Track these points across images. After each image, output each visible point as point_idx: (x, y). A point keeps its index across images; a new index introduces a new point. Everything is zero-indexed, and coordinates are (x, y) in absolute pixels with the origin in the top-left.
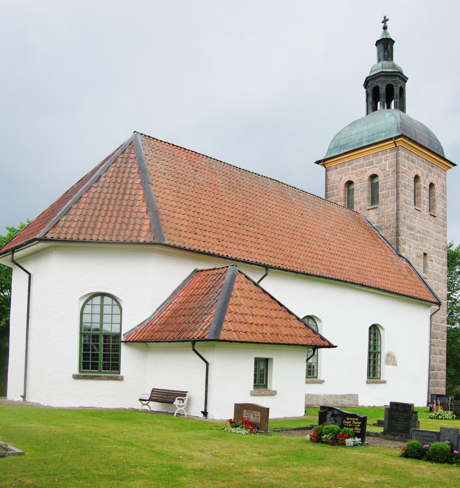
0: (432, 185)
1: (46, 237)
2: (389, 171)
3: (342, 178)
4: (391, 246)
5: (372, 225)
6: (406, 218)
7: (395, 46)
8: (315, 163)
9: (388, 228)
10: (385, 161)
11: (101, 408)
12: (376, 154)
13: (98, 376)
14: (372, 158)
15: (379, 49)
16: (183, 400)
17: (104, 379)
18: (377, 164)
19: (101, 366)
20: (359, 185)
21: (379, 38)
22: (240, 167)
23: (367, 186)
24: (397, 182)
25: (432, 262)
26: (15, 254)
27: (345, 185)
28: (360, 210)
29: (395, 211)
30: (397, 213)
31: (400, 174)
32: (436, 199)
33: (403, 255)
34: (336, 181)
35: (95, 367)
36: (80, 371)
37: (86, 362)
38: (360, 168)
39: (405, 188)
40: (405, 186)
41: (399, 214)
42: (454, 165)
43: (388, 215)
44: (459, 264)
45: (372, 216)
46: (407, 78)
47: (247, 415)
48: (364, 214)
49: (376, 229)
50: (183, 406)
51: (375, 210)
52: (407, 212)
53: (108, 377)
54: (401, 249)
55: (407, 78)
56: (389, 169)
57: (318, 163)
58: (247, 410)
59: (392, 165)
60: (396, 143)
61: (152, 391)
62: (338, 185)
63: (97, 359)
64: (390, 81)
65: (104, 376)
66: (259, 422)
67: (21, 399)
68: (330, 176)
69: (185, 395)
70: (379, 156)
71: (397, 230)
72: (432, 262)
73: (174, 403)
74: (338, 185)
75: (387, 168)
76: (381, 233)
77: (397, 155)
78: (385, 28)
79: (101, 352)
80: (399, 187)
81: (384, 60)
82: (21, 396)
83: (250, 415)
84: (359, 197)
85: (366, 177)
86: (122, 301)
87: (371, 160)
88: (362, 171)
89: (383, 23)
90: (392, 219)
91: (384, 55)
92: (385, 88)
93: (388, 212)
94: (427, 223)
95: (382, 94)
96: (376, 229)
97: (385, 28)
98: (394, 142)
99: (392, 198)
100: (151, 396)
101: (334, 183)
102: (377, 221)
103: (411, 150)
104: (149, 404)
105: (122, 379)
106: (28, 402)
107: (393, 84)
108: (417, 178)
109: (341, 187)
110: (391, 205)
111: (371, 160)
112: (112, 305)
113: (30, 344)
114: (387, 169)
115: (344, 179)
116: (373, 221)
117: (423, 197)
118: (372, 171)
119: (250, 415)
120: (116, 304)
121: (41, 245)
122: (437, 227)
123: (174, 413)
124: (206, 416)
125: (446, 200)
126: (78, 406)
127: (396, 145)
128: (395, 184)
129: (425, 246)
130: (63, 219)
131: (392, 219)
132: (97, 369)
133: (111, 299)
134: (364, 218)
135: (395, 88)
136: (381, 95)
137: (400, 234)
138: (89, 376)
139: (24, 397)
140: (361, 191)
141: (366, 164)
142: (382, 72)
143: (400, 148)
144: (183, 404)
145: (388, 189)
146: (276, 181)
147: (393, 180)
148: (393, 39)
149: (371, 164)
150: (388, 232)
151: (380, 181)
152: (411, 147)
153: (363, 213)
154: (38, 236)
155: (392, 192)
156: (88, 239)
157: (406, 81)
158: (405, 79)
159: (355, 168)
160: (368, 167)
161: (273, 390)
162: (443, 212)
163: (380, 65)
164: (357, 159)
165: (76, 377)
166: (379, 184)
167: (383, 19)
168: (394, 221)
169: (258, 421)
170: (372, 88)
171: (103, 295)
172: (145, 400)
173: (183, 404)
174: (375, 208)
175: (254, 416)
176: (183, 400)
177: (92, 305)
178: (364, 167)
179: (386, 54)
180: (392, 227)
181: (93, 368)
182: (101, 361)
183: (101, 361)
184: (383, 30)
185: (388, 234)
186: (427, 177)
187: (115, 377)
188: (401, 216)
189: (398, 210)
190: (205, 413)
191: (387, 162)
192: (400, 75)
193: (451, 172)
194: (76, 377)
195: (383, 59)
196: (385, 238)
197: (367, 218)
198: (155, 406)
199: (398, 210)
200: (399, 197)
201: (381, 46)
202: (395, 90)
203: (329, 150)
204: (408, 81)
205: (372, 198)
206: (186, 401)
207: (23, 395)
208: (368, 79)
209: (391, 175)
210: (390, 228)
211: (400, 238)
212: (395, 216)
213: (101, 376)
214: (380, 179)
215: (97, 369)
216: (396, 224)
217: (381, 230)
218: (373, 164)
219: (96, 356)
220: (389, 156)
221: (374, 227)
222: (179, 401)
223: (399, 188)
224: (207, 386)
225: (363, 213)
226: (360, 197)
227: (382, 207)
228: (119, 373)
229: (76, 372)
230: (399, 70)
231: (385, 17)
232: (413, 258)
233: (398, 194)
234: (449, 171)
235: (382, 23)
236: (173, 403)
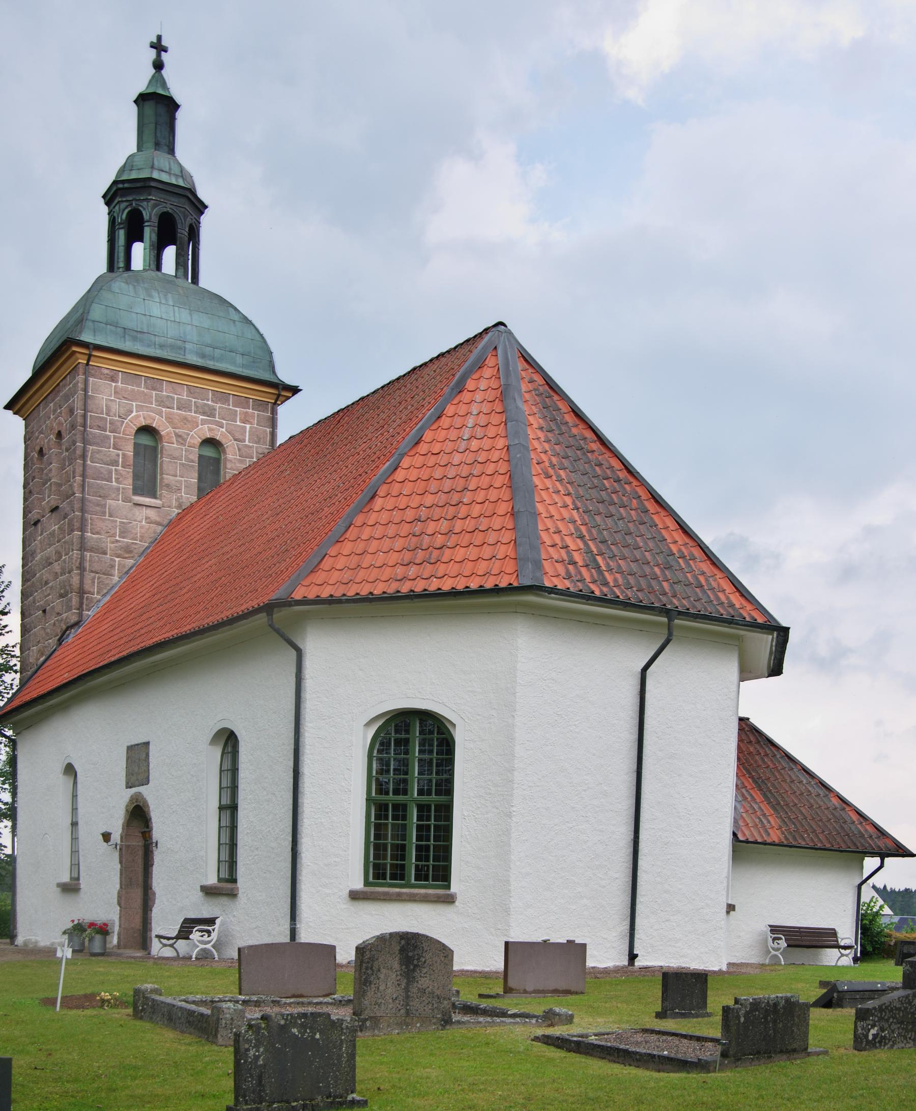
1: (292, 598)
2: (251, 447)
12: (222, 398)
16: (209, 932)
35: (399, 874)
36: (367, 883)
46: (206, 207)
50: (209, 942)
55: (206, 207)
60: (92, 358)
78: (158, 66)
85: (196, 436)
97: (158, 66)
105: (450, 900)
115: (137, 417)
118: (210, 430)
127: (88, 361)
139: (293, 933)
144: (209, 939)
148: (178, 99)
157: (202, 213)
158: (200, 207)
173: (209, 939)
176: (209, 932)
181: (393, 877)
184: (154, 71)
192: (190, 196)
219: (400, 851)
222: (200, 934)
228: (448, 887)
229: (358, 884)
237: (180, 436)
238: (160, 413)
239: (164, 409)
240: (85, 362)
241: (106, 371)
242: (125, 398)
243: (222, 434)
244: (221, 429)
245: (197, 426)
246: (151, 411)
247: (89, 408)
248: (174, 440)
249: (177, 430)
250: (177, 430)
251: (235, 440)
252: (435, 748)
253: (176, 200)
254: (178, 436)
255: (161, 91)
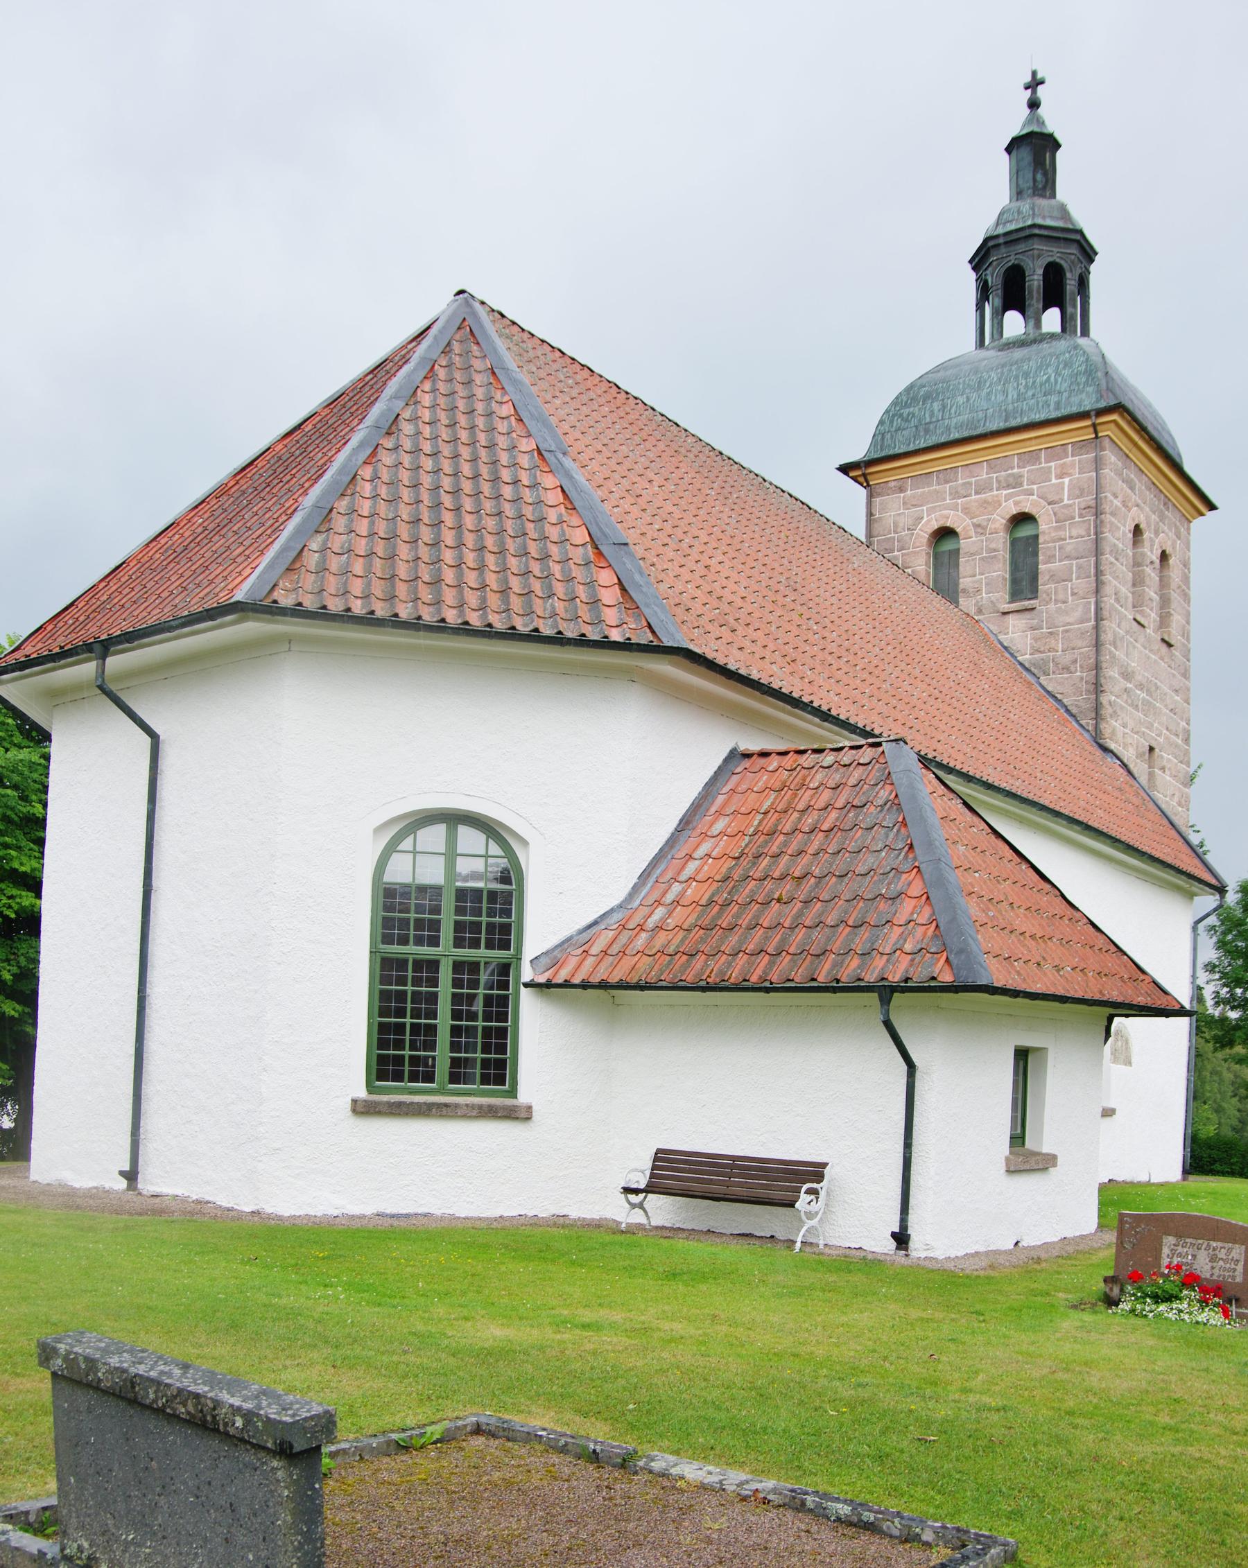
0: (1164, 556)
1: (275, 602)
2: (1071, 505)
3: (922, 518)
4: (1077, 721)
5: (1015, 658)
6: (1118, 643)
7: (1060, 155)
8: (838, 469)
9: (1066, 669)
10: (1060, 476)
11: (454, 1218)
12: (1033, 457)
13: (446, 1105)
14: (1019, 467)
15: (1018, 162)
17: (465, 1117)
18: (1033, 483)
19: (442, 1069)
20: (974, 542)
21: (1016, 130)
22: (720, 449)
23: (1001, 546)
24: (1097, 541)
25: (1164, 772)
26: (109, 660)
27: (929, 540)
28: (980, 611)
29: (1088, 620)
30: (1097, 628)
31: (1107, 518)
32: (1172, 598)
33: (1112, 746)
34: (901, 525)
37: (388, 1056)
38: (977, 493)
39: (1117, 559)
40: (1116, 553)
41: (1104, 632)
42: (1212, 507)
43: (1067, 631)
44: (7, 819)
45: (1016, 632)
47: (1180, 1255)
48: (992, 627)
49: (1027, 670)
51: (1027, 615)
52: (1119, 626)
53: (480, 1107)
54: (1106, 728)
55: (1096, 254)
56: (1071, 502)
57: (845, 469)
58: (1179, 1235)
59: (1082, 491)
60: (1099, 428)
61: (656, 1159)
62: (907, 538)
63: (431, 1046)
64: (1054, 253)
65: (467, 1105)
66: (1239, 1279)
67: (122, 1184)
68: (883, 510)
69: (819, 1177)
70: (1040, 463)
71: (1097, 676)
72: (1164, 772)
73: (797, 1205)
74: (908, 538)
75: (1066, 497)
76: (1044, 683)
77: (1098, 464)
78: (1034, 104)
79: (444, 1021)
80: (1102, 554)
81: (1034, 194)
82: (122, 1173)
83: (1194, 1256)
84: (975, 576)
85: (999, 520)
86: (525, 843)
87: (1016, 470)
88: (985, 502)
89: (1029, 91)
90: (1079, 643)
91: (1035, 180)
92: (1041, 271)
93: (1069, 624)
94: (1155, 661)
95: (1035, 288)
96: (1027, 670)
97: (1034, 104)
98: (1094, 426)
99: (1084, 584)
100: (652, 1176)
101: (896, 532)
102: (1032, 647)
103: (1130, 455)
104: (646, 1205)
105: (520, 1115)
106: (145, 1192)
107: (1062, 262)
108: (1137, 531)
109: (918, 544)
110: (1077, 605)
111: (1016, 470)
112: (487, 856)
113: (154, 991)
114: (1066, 502)
115: (928, 521)
116: (1020, 646)
117: (1148, 586)
118: (1016, 503)
119: (1194, 1256)
120: (500, 853)
121: (252, 627)
122: (1174, 675)
123: (794, 1242)
124: (906, 1249)
125: (1189, 602)
126: (369, 1210)
127: (1096, 432)
128: (1091, 546)
129: (1150, 727)
130: (314, 546)
131: (1079, 643)
132: (429, 1078)
133: (484, 836)
134: (992, 637)
135: (1068, 275)
136: (1031, 292)
137: (1105, 688)
138: (412, 1103)
139: (131, 1176)
140: (982, 559)
141: (998, 481)
142: (1034, 226)
143: (1106, 442)
145: (1068, 557)
146: (803, 503)
147: (1084, 533)
148: (1059, 136)
149: (1015, 482)
150: (1067, 679)
151: (1044, 533)
152: (1130, 446)
153: (990, 624)
154: (239, 596)
155: (1079, 567)
156: (429, 619)
158: (1088, 253)
159: (963, 492)
160: (1005, 492)
161: (1045, 1150)
162: (1183, 636)
163: (1025, 206)
164: (970, 467)
165: (362, 1109)
166: (1041, 540)
167: (1028, 79)
168: (1084, 648)
169: (1234, 1277)
170: (1003, 270)
171: (454, 819)
172: (636, 1191)
174: (1026, 610)
175: (1213, 1259)
177: (415, 852)
178: (991, 490)
179: (1039, 177)
180: (1081, 667)
182: (442, 1054)
183: (442, 1054)
184: (1029, 111)
185: (1071, 687)
186: (1157, 533)
187: (505, 1108)
188: (1107, 637)
189: (1099, 618)
190: (901, 1239)
191: (1066, 480)
193: (1203, 525)
194: (362, 1109)
195: (1030, 191)
196: (1059, 696)
197: (1001, 637)
198: (662, 1210)
199: (1099, 618)
200: (1103, 583)
201: (1025, 153)
202: (1068, 282)
203: (879, 436)
204: (1097, 258)
205: (1015, 582)
206: (822, 1194)
207: (127, 1168)
208: (990, 244)
209: (1077, 519)
210: (1072, 669)
211: (1104, 699)
212: (1089, 638)
213: (457, 1106)
214: (1045, 525)
215: (431, 1080)
216: (1092, 660)
217: (1046, 674)
218: (1021, 485)
220: (1072, 465)
221: (1021, 664)
223: (1104, 557)
224: (908, 1145)
225: (989, 622)
226: (978, 577)
227: (1046, 607)
228: (513, 1093)
229: (362, 1093)
230: (1073, 224)
231: (1034, 74)
232: (1128, 755)
233: (1098, 573)
234: (1198, 523)
235: (1026, 88)
236: (793, 1206)
237: (979, 526)
238: (955, 508)
239: (959, 501)
240: (1093, 436)
241: (893, 484)
242: (914, 506)
243: (1034, 504)
244: (1031, 497)
245: (1000, 505)
246: (945, 509)
247: (875, 533)
248: (972, 533)
249: (975, 520)
250: (975, 520)
251: (1049, 504)
252: (497, 919)
253: (1023, 246)
254: (976, 526)
255: (1036, 129)
